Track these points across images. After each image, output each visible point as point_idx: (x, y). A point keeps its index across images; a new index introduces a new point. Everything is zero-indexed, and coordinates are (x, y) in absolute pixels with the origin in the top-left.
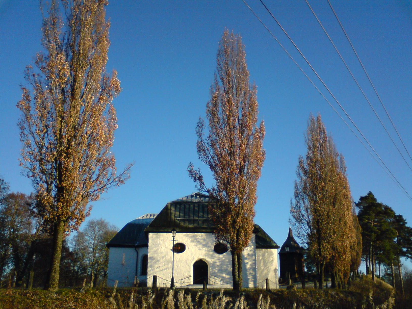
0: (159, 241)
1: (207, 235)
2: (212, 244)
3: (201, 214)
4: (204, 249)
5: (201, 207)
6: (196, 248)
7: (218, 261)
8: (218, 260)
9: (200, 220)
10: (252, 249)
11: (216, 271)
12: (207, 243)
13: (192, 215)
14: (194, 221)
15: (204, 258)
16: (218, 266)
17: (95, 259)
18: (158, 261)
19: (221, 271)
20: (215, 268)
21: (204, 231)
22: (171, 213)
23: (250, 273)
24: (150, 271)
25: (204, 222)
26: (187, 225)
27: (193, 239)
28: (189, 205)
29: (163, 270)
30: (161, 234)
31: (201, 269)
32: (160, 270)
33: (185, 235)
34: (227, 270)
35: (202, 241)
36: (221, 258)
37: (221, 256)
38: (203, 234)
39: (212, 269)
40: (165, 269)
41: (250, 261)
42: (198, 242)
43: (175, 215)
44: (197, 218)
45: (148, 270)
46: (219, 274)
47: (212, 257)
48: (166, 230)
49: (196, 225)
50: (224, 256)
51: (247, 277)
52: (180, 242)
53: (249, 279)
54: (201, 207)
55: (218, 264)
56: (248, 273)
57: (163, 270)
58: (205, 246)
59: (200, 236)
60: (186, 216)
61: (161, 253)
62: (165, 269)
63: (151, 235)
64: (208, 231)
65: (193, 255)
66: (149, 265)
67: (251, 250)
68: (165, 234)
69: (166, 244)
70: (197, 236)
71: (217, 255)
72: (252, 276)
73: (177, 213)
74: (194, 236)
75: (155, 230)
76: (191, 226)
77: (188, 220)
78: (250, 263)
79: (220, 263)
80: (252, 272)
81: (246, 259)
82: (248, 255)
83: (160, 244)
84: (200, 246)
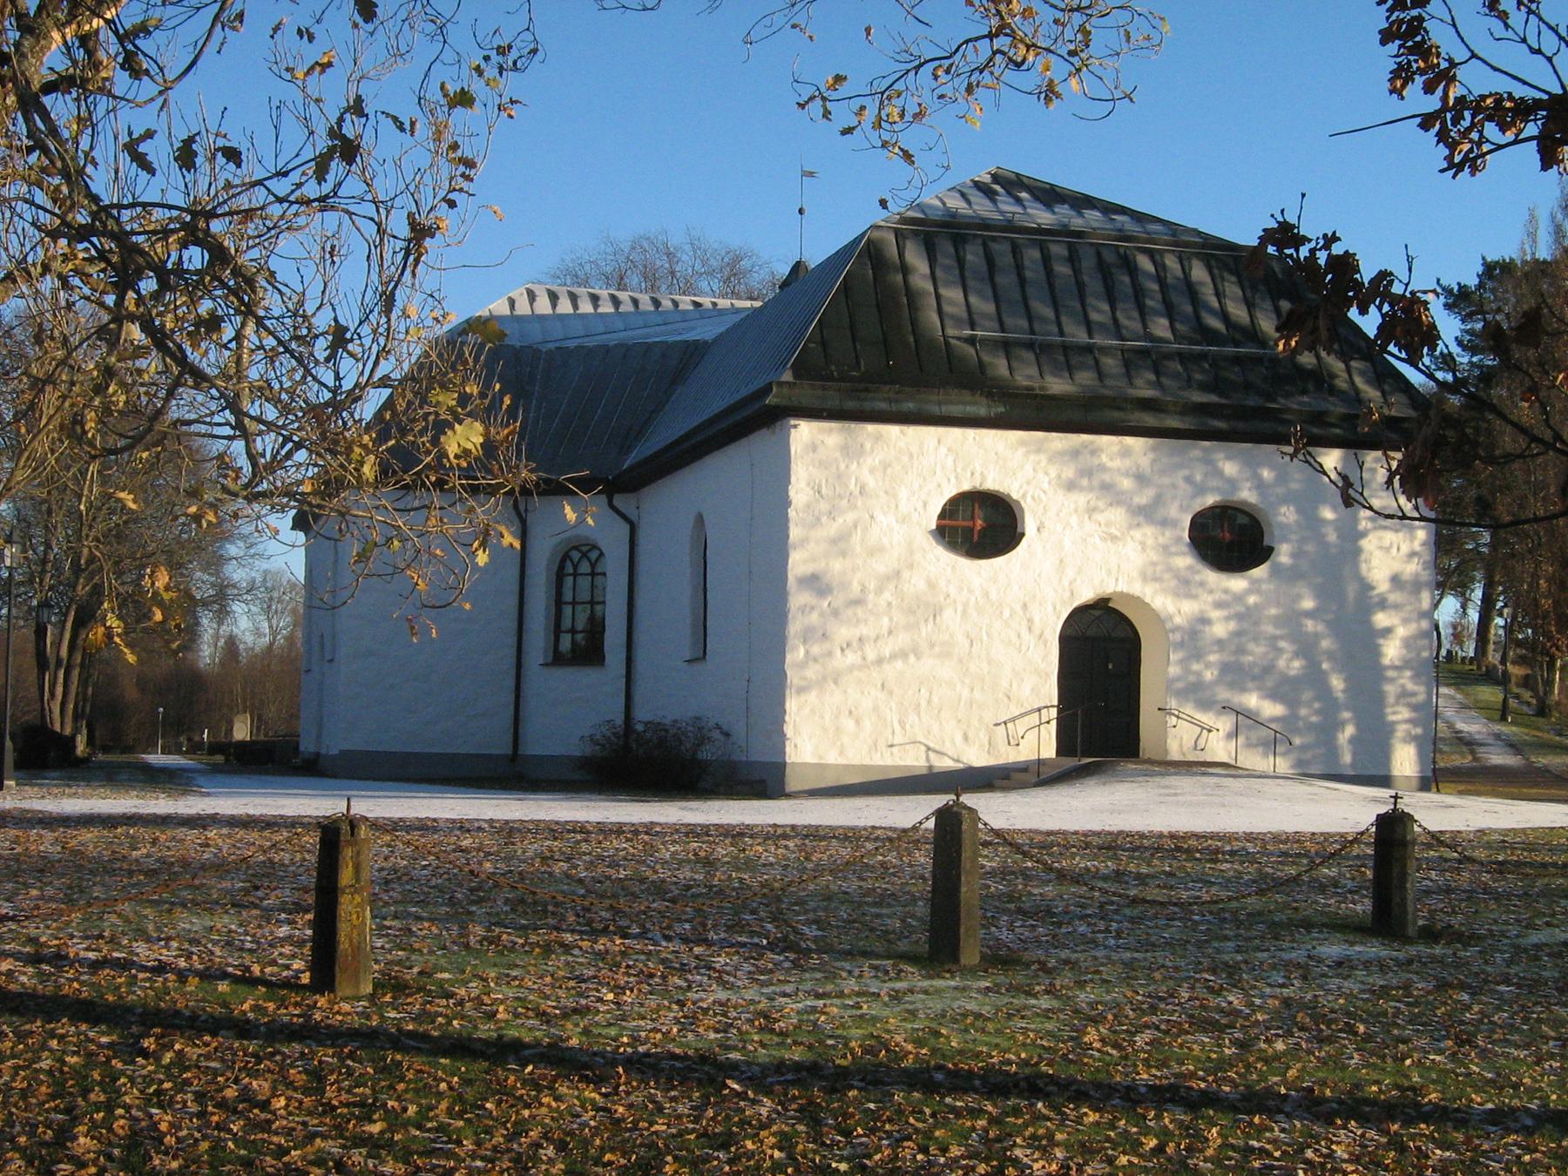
0: (864, 472)
1: (1154, 449)
2: (1182, 508)
3: (1100, 312)
4: (1137, 534)
5: (1088, 263)
6: (1089, 526)
7: (1215, 614)
8: (1219, 605)
9: (1104, 350)
10: (1417, 547)
11: (1209, 675)
12: (1158, 500)
13: (1049, 313)
14: (1068, 356)
15: (1136, 589)
16: (1220, 644)
17: (1508, 441)
18: (858, 602)
19: (1236, 675)
20: (1198, 655)
21: (1150, 420)
22: (911, 294)
23: (1404, 694)
24: (802, 665)
25: (1133, 360)
26: (1026, 375)
27: (1069, 472)
28: (1016, 250)
29: (880, 661)
30: (871, 428)
31: (1102, 668)
32: (864, 665)
33: (1022, 443)
34: (1268, 669)
35: (1127, 484)
36: (1239, 598)
37: (1237, 583)
38: (1130, 441)
39: (1183, 662)
40: (893, 657)
41: (1405, 621)
42: (1106, 488)
43: (946, 305)
44: (1081, 336)
45: (789, 658)
46: (1223, 694)
47: (1185, 588)
48: (910, 406)
49: (1086, 378)
50: (1254, 582)
51: (1382, 716)
52: (991, 484)
53: (1389, 729)
54: (1088, 263)
55: (1220, 630)
56: (1391, 690)
57: (880, 661)
58: (1147, 514)
59: (1121, 455)
60: (1009, 321)
61: (876, 551)
62: (893, 657)
63: (803, 433)
64: (1173, 422)
65: (1070, 573)
66: (794, 627)
67: (1413, 554)
68: (893, 431)
69: (903, 494)
70: (1095, 452)
71: (1212, 577)
72: (1415, 708)
73: (953, 294)
74: (1075, 453)
75: (834, 402)
76: (1057, 385)
77: (1030, 346)
78: (1401, 632)
79: (1232, 626)
80: (1410, 686)
81: (1383, 604)
82: (1396, 580)
83: (861, 492)
84: (1117, 515)
